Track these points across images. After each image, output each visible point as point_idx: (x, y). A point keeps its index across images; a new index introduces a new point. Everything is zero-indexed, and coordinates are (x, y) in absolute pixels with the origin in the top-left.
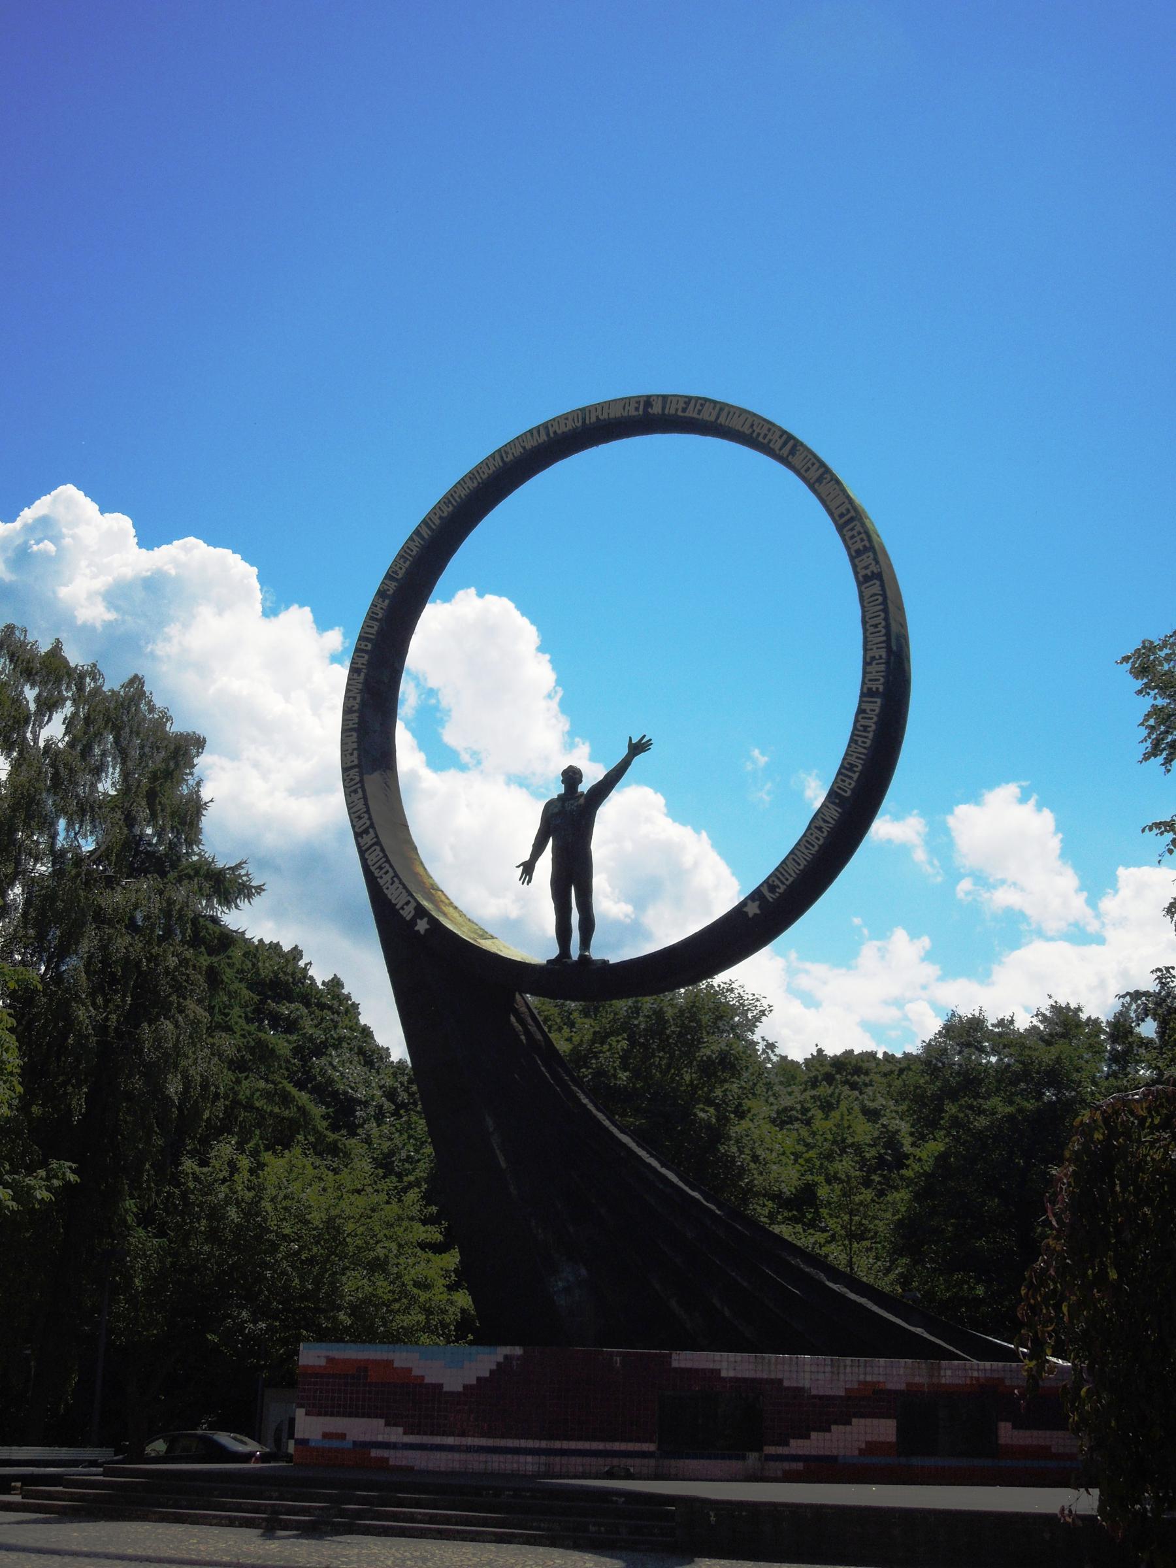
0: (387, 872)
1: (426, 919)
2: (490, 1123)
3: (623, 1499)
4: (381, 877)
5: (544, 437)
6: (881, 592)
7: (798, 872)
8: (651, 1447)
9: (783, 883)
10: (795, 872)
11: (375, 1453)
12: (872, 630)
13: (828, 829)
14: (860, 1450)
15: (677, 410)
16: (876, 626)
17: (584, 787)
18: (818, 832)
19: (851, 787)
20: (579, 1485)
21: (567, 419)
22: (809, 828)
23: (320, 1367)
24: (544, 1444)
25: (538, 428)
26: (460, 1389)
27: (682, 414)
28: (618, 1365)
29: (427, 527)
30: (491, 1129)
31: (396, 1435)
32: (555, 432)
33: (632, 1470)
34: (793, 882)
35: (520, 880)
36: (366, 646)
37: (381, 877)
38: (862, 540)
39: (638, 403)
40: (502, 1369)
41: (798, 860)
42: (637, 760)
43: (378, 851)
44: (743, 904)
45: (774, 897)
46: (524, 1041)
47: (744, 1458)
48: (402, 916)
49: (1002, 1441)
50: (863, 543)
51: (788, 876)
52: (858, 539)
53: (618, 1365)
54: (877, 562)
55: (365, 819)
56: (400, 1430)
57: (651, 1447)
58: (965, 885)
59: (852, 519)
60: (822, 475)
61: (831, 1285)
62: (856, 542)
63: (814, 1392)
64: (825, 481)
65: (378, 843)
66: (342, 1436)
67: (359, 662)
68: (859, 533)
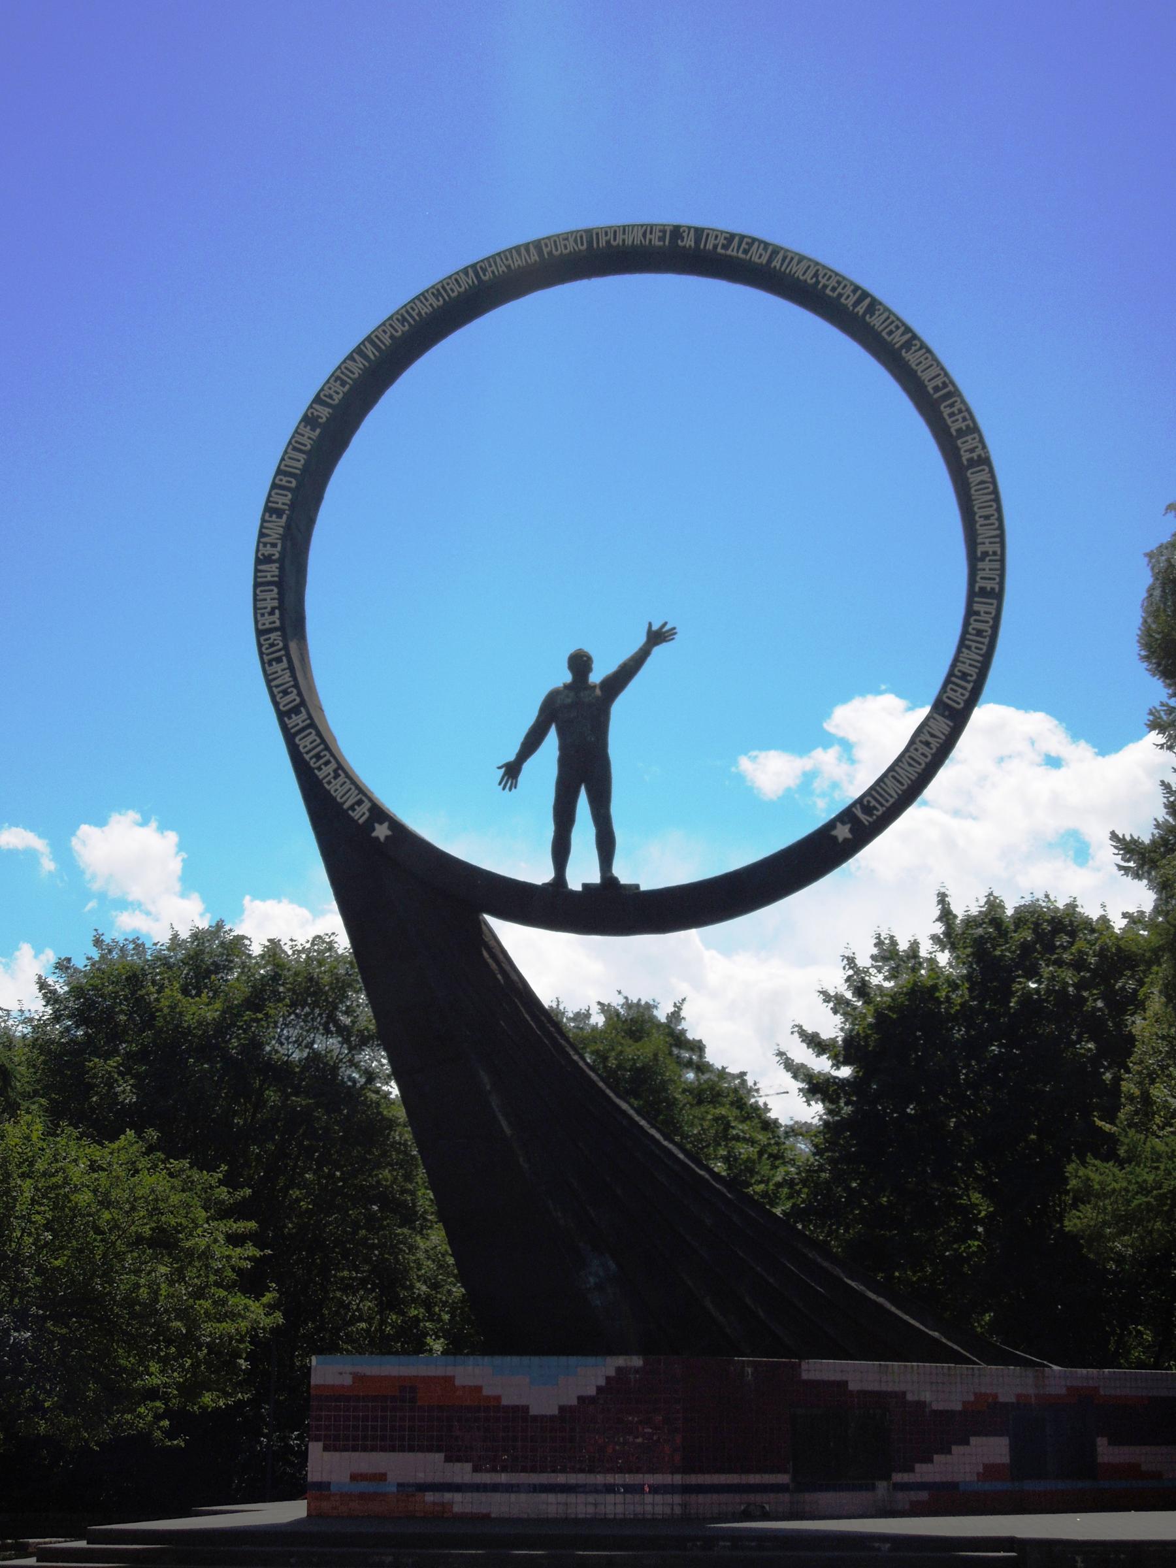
0: (327, 763)
1: (386, 825)
2: (486, 1080)
3: (888, 1546)
5: (535, 257)
6: (990, 480)
7: (900, 792)
8: (784, 1479)
9: (882, 805)
10: (896, 792)
13: (938, 745)
14: (978, 1474)
15: (715, 247)
16: (987, 517)
17: (596, 677)
18: (925, 748)
19: (965, 698)
20: (793, 1530)
21: (567, 239)
22: (912, 742)
23: (343, 1386)
25: (527, 246)
27: (723, 251)
28: (750, 1377)
29: (373, 346)
30: (488, 1087)
31: (462, 1472)
33: (767, 1507)
35: (500, 784)
36: (290, 482)
40: (615, 1386)
41: (900, 779)
42: (657, 651)
43: (313, 736)
44: (831, 825)
45: (870, 819)
46: (502, 981)
47: (873, 1488)
49: (1100, 1460)
50: (966, 423)
51: (888, 798)
52: (959, 417)
53: (750, 1377)
55: (294, 695)
56: (468, 1467)
57: (784, 1479)
58: (92, 905)
61: (849, 1282)
62: (957, 420)
63: (935, 1407)
64: (914, 348)
65: (312, 725)
66: (382, 1477)
67: (280, 501)
68: (960, 411)
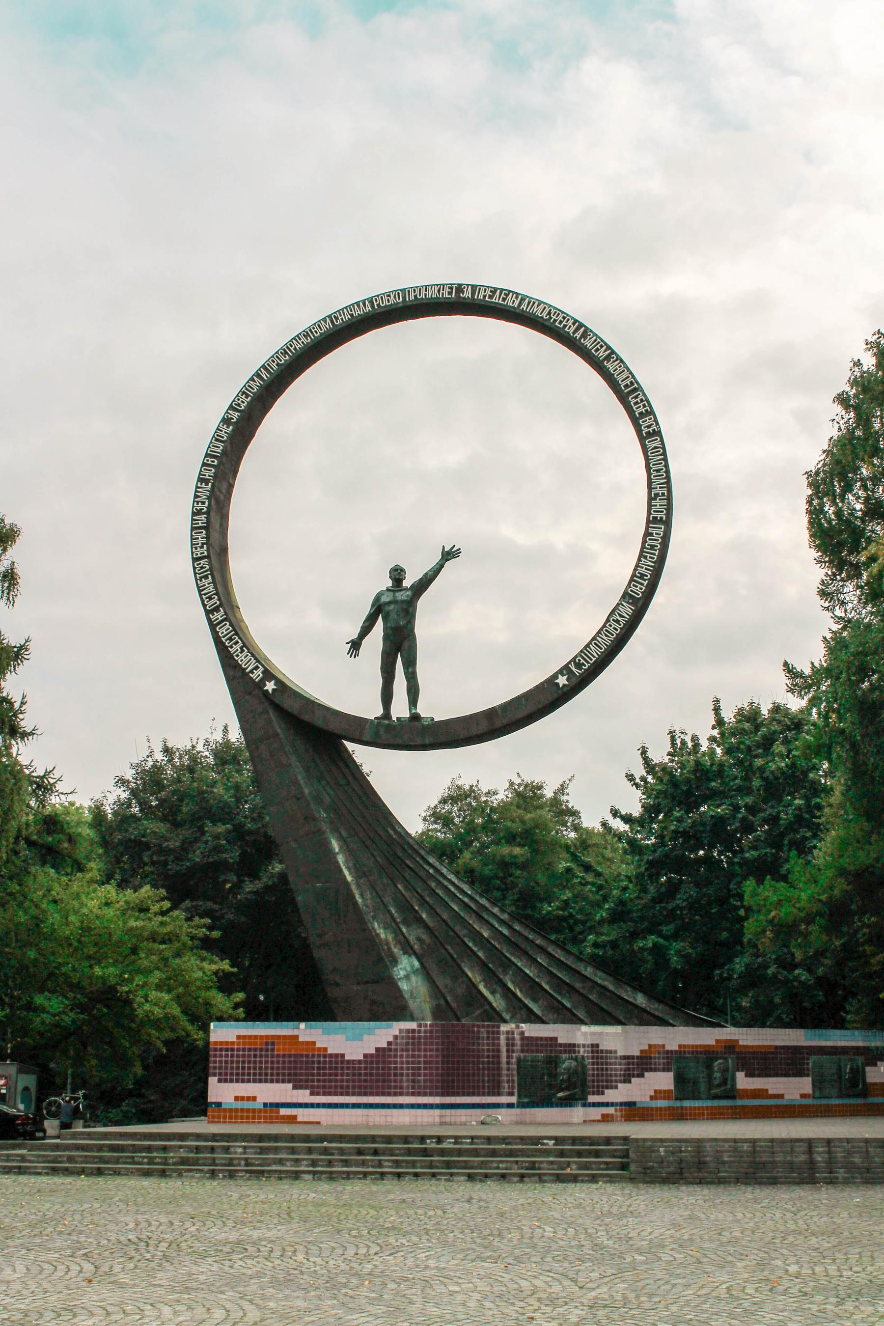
0: (237, 643)
2: (335, 845)
4: (231, 647)
5: (369, 308)
8: (514, 1099)
9: (588, 662)
11: (283, 1112)
12: (655, 474)
16: (658, 471)
17: (407, 583)
24: (437, 1100)
26: (361, 1058)
31: (303, 1096)
32: (379, 305)
34: (595, 661)
37: (231, 647)
38: (644, 406)
39: (451, 288)
48: (251, 678)
54: (657, 424)
59: (635, 390)
60: (609, 355)
